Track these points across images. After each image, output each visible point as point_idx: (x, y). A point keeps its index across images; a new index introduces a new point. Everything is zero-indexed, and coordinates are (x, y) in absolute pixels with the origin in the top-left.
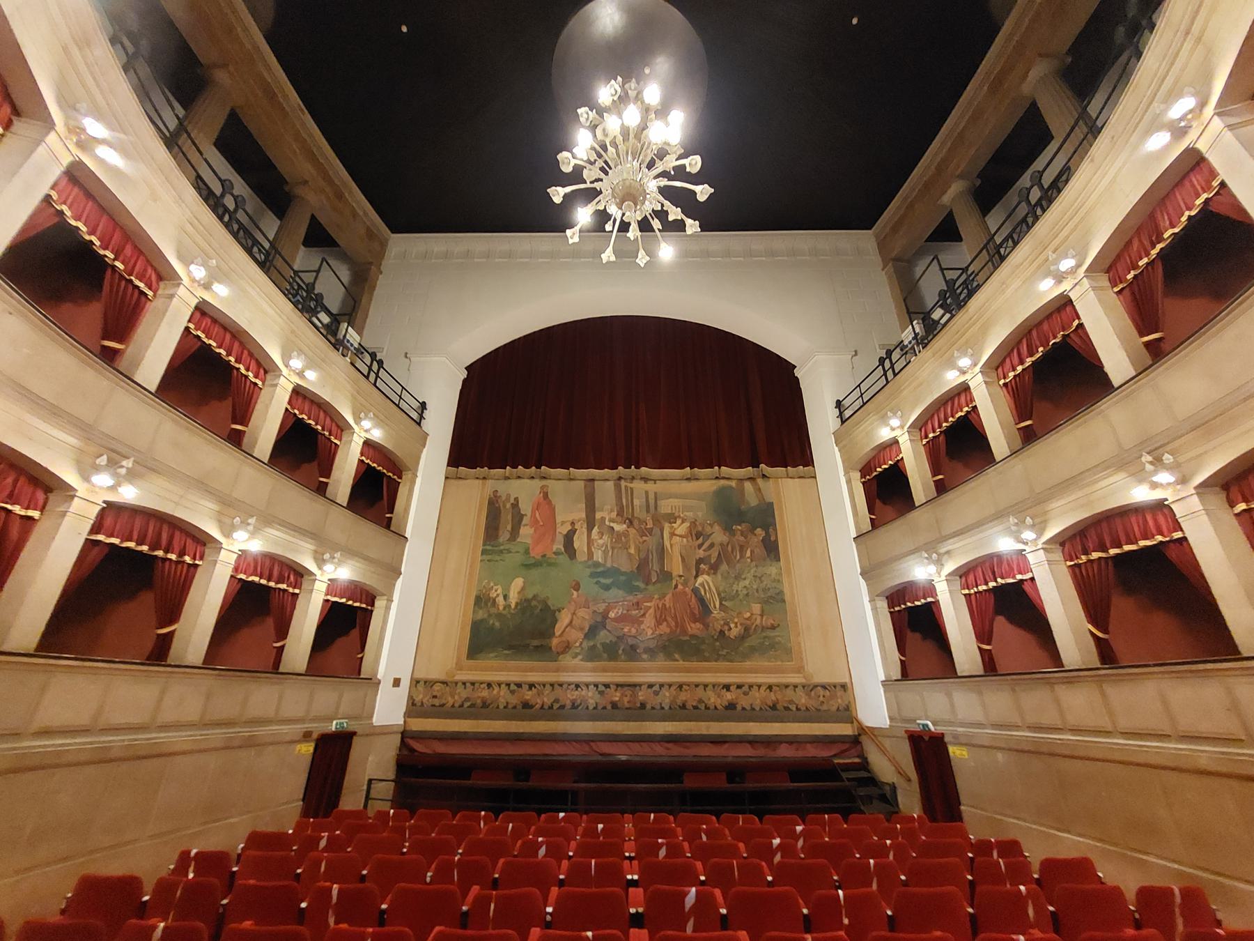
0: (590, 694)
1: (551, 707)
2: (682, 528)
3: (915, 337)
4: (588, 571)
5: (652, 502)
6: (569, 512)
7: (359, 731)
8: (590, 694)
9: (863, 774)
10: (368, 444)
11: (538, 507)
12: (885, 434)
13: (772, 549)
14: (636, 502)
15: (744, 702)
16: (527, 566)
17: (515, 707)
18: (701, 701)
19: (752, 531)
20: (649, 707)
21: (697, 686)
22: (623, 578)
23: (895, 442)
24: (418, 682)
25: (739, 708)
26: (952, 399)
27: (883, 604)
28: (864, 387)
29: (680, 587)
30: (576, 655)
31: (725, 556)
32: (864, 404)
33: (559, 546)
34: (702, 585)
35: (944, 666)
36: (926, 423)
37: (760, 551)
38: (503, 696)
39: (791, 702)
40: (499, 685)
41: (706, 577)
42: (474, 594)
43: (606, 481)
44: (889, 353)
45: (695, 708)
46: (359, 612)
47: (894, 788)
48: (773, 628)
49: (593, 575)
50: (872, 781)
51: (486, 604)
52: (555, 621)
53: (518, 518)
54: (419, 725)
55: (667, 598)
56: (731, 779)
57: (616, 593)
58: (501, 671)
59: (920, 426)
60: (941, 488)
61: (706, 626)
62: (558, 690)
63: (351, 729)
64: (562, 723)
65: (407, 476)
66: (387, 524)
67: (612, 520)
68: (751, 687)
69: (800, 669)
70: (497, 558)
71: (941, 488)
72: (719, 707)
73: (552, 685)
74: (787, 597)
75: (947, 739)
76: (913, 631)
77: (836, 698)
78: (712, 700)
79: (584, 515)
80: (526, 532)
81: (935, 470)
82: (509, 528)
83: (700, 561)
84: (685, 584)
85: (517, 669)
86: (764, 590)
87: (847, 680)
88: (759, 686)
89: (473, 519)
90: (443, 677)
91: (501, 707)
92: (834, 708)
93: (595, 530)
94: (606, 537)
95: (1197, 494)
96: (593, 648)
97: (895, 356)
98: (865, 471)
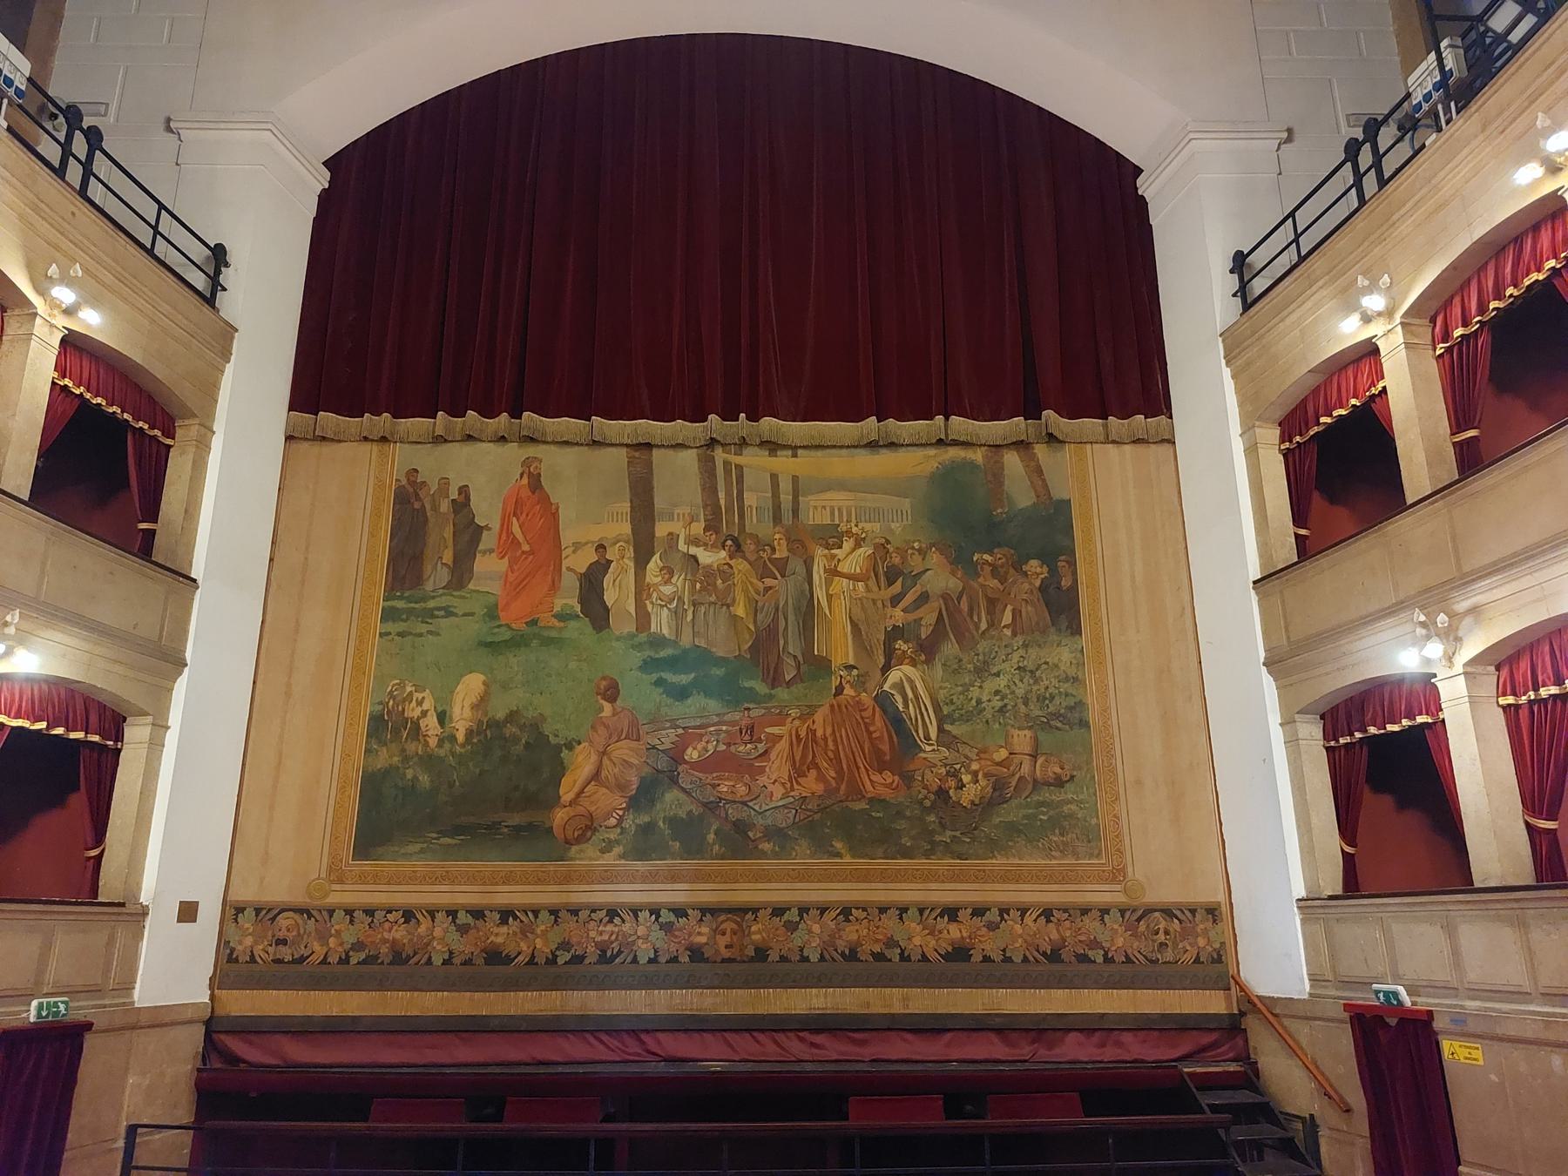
0: (641, 931)
1: (552, 961)
2: (853, 559)
3: (1442, 84)
4: (637, 658)
5: (786, 499)
6: (590, 519)
7: (99, 1024)
8: (641, 931)
9: (1243, 1097)
10: (73, 346)
11: (515, 508)
12: (1350, 331)
13: (1062, 607)
14: (750, 499)
15: (990, 944)
16: (492, 647)
17: (467, 962)
18: (891, 943)
19: (1018, 566)
20: (773, 956)
21: (883, 910)
22: (718, 672)
23: (1369, 352)
24: (240, 910)
25: (977, 957)
26: (1518, 240)
27: (1312, 732)
28: (1303, 218)
29: (848, 691)
30: (607, 848)
31: (952, 623)
32: (1302, 259)
33: (568, 599)
34: (899, 686)
36: (1448, 304)
38: (442, 938)
39: (1095, 944)
40: (432, 914)
41: (907, 669)
42: (366, 710)
43: (679, 452)
44: (1373, 127)
45: (879, 957)
46: (85, 752)
47: (1311, 1124)
48: (1059, 783)
49: (648, 665)
50: (1265, 1111)
51: (396, 732)
52: (559, 770)
53: (469, 534)
54: (244, 1003)
55: (819, 717)
56: (953, 1108)
57: (701, 706)
58: (433, 884)
59: (1435, 310)
60: (1471, 460)
61: (907, 778)
62: (569, 925)
63: (79, 1016)
64: (576, 995)
65: (186, 432)
66: (144, 547)
67: (695, 541)
68: (1004, 911)
69: (1117, 875)
70: (423, 628)
71: (1471, 460)
72: (932, 955)
73: (554, 912)
74: (1093, 717)
75: (1438, 1024)
76: (1378, 788)
77: (1196, 935)
78: (917, 941)
79: (626, 528)
80: (489, 567)
81: (1461, 416)
82: (448, 557)
83: (895, 633)
84: (860, 683)
85: (472, 879)
86: (1041, 699)
87: (1221, 897)
88: (1023, 911)
89: (357, 539)
90: (300, 899)
91: (437, 960)
92: (1189, 957)
93: (655, 563)
94: (678, 580)
95: (1465, 673)
96: (647, 829)
97: (1386, 136)
98: (1290, 424)
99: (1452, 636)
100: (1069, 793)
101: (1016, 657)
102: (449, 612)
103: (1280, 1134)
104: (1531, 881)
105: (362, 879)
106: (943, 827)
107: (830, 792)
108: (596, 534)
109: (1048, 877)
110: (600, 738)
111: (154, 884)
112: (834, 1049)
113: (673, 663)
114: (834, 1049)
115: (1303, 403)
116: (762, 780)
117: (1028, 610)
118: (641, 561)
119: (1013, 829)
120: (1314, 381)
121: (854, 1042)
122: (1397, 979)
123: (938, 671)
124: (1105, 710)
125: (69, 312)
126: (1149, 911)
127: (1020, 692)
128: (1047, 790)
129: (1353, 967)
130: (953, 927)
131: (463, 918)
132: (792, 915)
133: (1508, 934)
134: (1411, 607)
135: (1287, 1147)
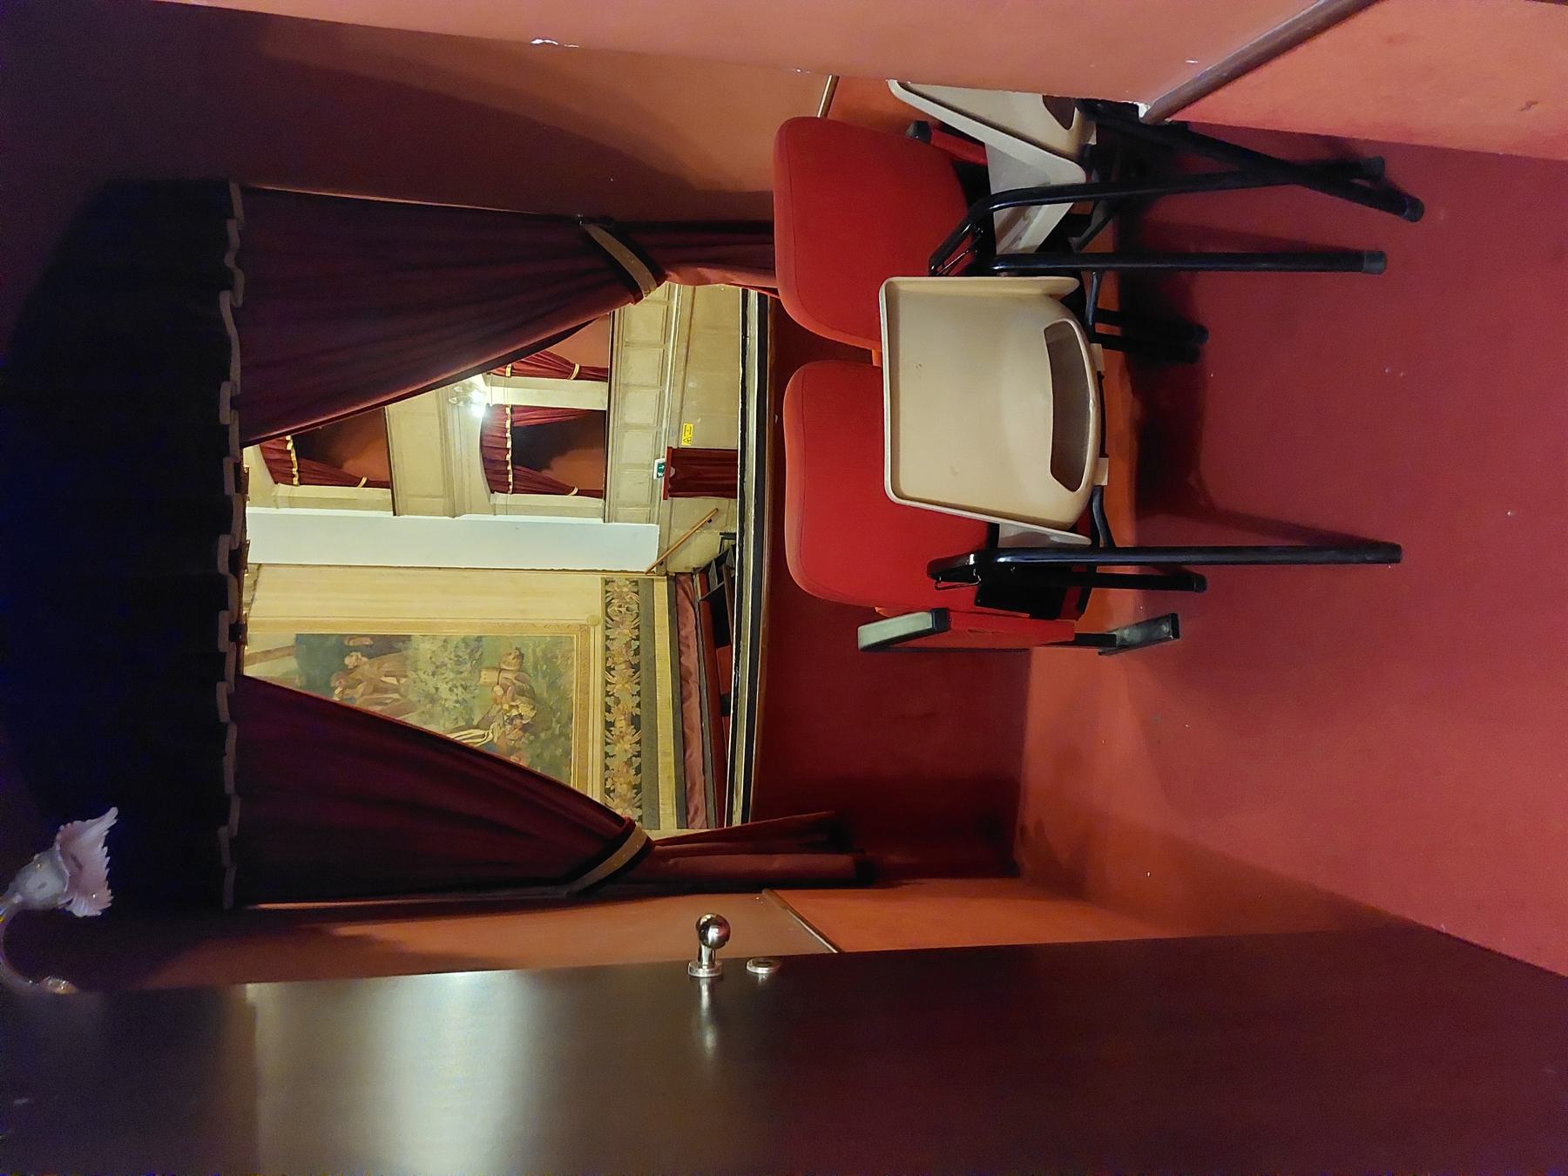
9: (713, 571)
15: (629, 703)
18: (629, 763)
19: (348, 671)
25: (638, 711)
27: (500, 498)
37: (389, 663)
39: (628, 645)
45: (638, 770)
68: (608, 694)
69: (584, 630)
74: (475, 633)
78: (627, 747)
86: (459, 663)
92: (635, 597)
100: (529, 653)
101: (424, 677)
106: (549, 728)
109: (585, 667)
117: (386, 667)
119: (552, 686)
121: (692, 788)
122: (651, 466)
127: (452, 676)
129: (643, 493)
130: (618, 724)
133: (633, 396)
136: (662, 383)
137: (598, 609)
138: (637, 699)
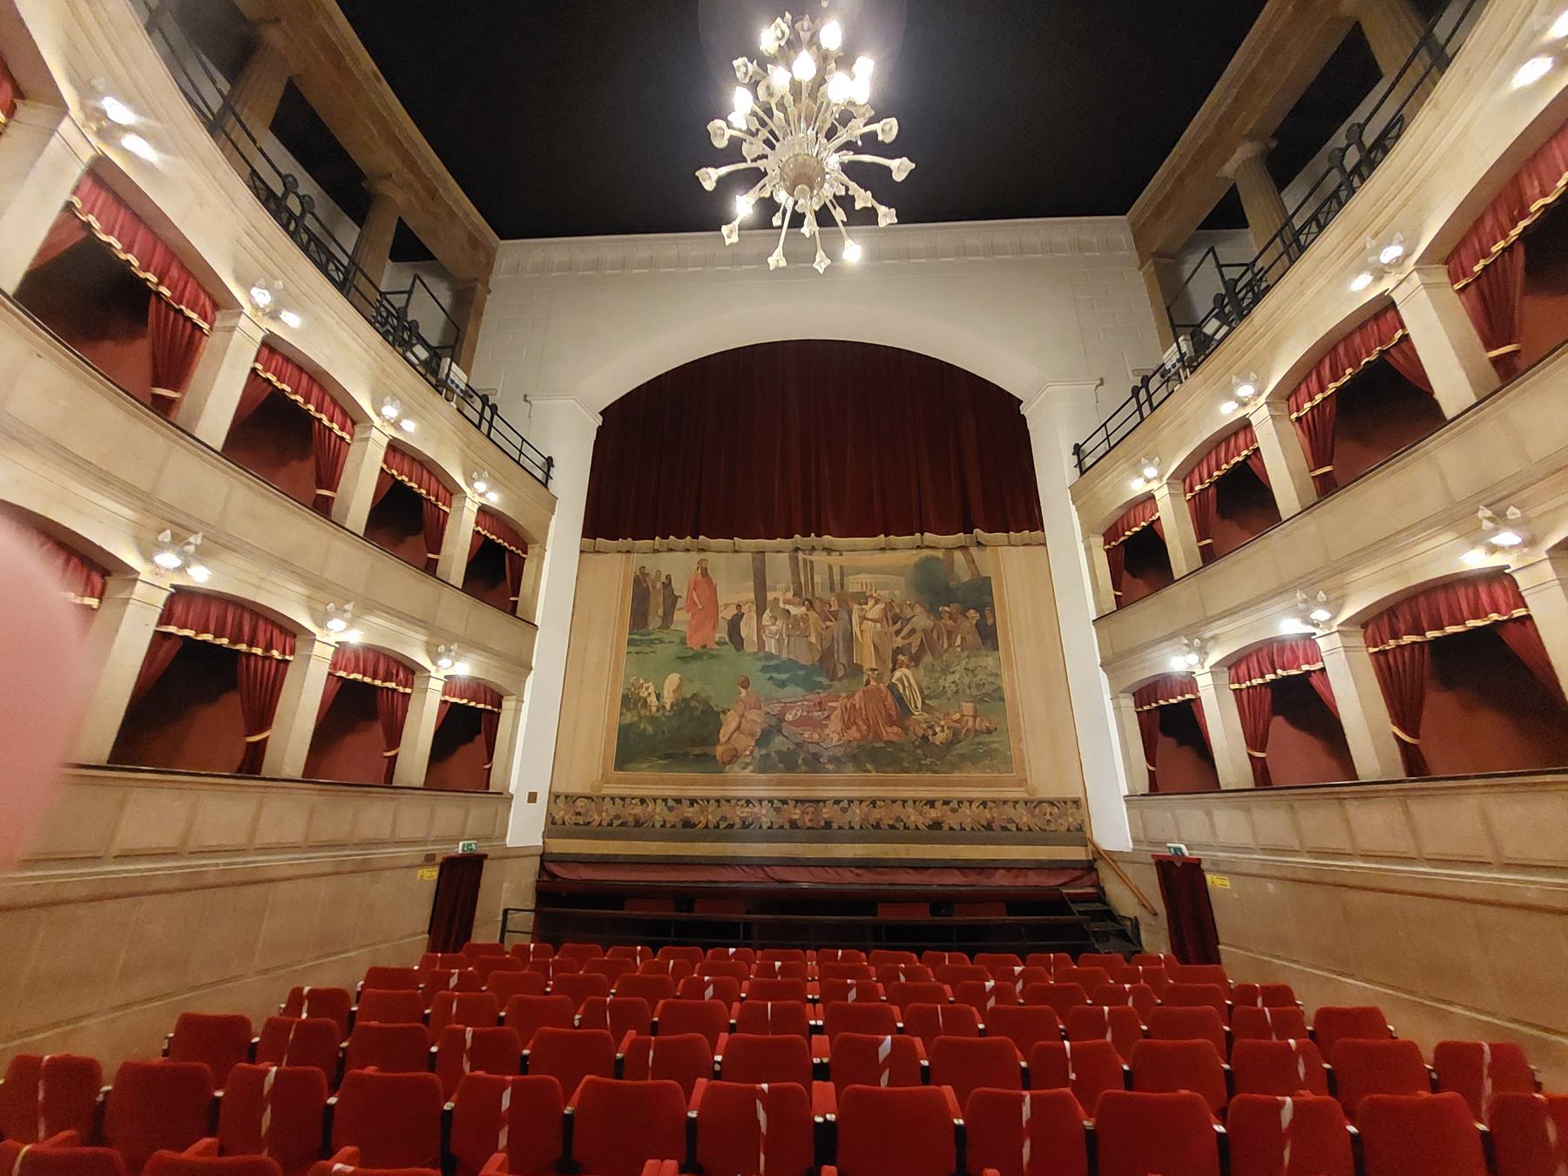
1: (717, 827)
2: (874, 611)
3: (1181, 359)
4: (759, 665)
5: (837, 578)
6: (734, 592)
10: (484, 511)
12: (1137, 487)
13: (988, 635)
14: (817, 579)
15: (952, 820)
18: (899, 819)
19: (964, 613)
20: (835, 826)
21: (894, 801)
24: (557, 797)
25: (946, 827)
26: (1227, 440)
27: (1128, 703)
28: (1111, 426)
29: (873, 683)
32: (1111, 448)
33: (722, 634)
35: (1204, 776)
37: (974, 638)
38: (659, 813)
39: (1011, 820)
40: (655, 800)
41: (905, 670)
43: (778, 553)
44: (1146, 381)
45: (892, 827)
47: (1136, 923)
48: (989, 732)
49: (765, 669)
50: (1109, 914)
51: (635, 704)
52: (719, 725)
53: (671, 600)
56: (935, 911)
57: (793, 691)
58: (656, 785)
59: (1184, 476)
60: (1209, 556)
61: (905, 729)
62: (725, 807)
63: (481, 851)
66: (512, 609)
67: (788, 602)
68: (960, 802)
69: (1022, 782)
71: (1209, 556)
73: (718, 801)
74: (1007, 695)
75: (1204, 866)
79: (752, 596)
80: (681, 617)
81: (1202, 531)
82: (660, 612)
83: (898, 651)
86: (978, 686)
87: (1081, 795)
88: (971, 802)
89: (614, 604)
90: (587, 791)
91: (658, 825)
92: (1065, 827)
93: (767, 615)
94: (779, 623)
97: (1154, 384)
98: (1109, 535)
99: (1203, 651)
102: (661, 641)
103: (1118, 927)
104: (1252, 786)
105: (619, 781)
107: (863, 737)
108: (736, 599)
110: (740, 707)
111: (516, 784)
112: (868, 877)
113: (777, 668)
114: (868, 877)
115: (1115, 524)
116: (827, 731)
118: (760, 614)
119: (963, 757)
120: (1122, 512)
122: (1180, 841)
123: (921, 671)
124: (1014, 692)
125: (481, 495)
126: (1041, 802)
128: (982, 739)
129: (1156, 834)
131: (671, 803)
132: (845, 804)
133: (1240, 816)
134: (1295, 589)
135: (1122, 934)
136: (1264, 850)
137: (1042, 795)
138: (957, 827)
